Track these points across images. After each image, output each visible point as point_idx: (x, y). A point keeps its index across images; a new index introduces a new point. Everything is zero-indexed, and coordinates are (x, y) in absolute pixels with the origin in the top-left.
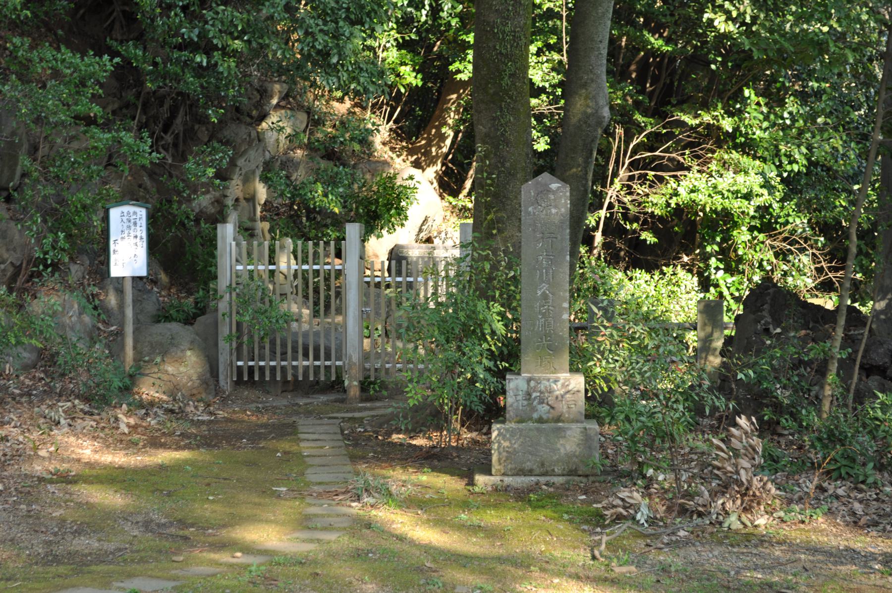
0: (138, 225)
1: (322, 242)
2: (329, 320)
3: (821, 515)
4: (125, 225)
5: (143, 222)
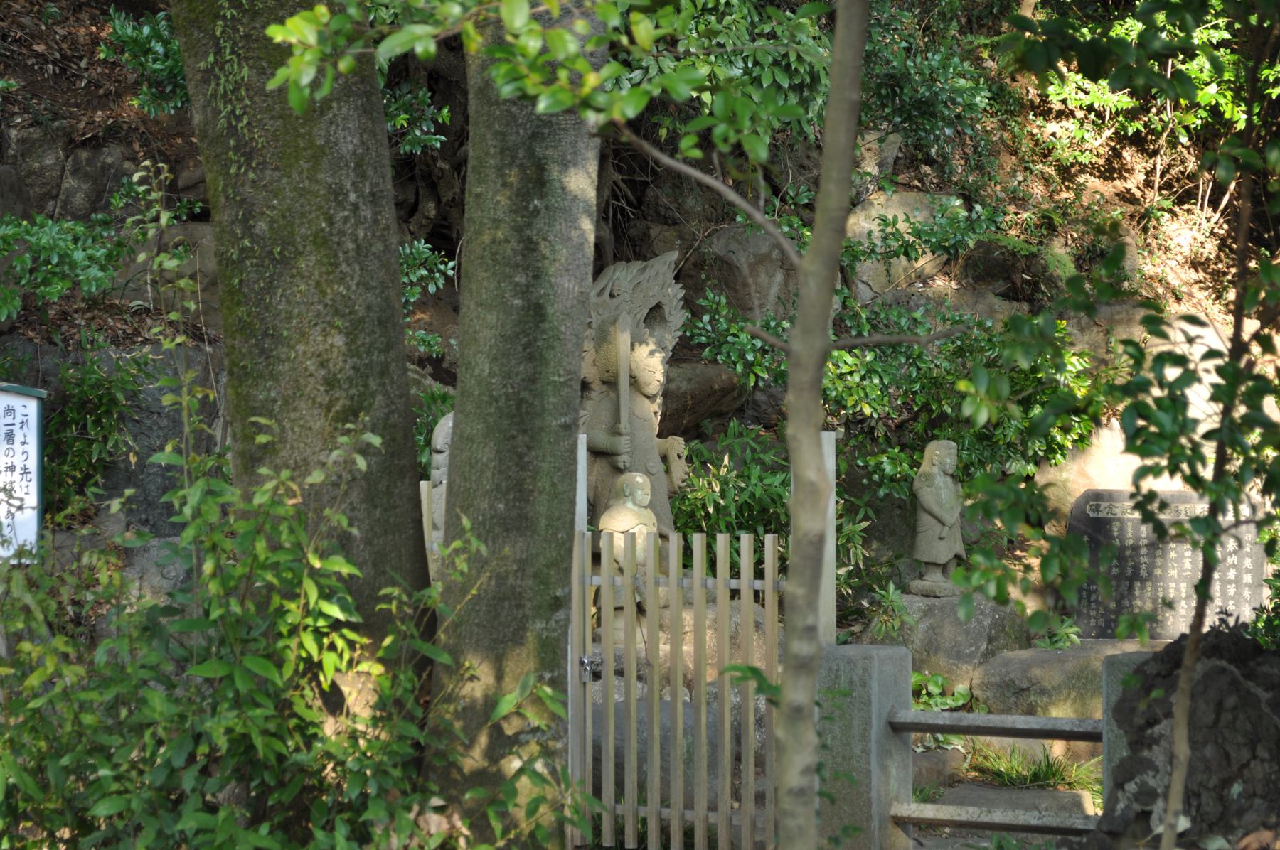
0: (19, 438)
2: (543, 522)
3: (282, 73)
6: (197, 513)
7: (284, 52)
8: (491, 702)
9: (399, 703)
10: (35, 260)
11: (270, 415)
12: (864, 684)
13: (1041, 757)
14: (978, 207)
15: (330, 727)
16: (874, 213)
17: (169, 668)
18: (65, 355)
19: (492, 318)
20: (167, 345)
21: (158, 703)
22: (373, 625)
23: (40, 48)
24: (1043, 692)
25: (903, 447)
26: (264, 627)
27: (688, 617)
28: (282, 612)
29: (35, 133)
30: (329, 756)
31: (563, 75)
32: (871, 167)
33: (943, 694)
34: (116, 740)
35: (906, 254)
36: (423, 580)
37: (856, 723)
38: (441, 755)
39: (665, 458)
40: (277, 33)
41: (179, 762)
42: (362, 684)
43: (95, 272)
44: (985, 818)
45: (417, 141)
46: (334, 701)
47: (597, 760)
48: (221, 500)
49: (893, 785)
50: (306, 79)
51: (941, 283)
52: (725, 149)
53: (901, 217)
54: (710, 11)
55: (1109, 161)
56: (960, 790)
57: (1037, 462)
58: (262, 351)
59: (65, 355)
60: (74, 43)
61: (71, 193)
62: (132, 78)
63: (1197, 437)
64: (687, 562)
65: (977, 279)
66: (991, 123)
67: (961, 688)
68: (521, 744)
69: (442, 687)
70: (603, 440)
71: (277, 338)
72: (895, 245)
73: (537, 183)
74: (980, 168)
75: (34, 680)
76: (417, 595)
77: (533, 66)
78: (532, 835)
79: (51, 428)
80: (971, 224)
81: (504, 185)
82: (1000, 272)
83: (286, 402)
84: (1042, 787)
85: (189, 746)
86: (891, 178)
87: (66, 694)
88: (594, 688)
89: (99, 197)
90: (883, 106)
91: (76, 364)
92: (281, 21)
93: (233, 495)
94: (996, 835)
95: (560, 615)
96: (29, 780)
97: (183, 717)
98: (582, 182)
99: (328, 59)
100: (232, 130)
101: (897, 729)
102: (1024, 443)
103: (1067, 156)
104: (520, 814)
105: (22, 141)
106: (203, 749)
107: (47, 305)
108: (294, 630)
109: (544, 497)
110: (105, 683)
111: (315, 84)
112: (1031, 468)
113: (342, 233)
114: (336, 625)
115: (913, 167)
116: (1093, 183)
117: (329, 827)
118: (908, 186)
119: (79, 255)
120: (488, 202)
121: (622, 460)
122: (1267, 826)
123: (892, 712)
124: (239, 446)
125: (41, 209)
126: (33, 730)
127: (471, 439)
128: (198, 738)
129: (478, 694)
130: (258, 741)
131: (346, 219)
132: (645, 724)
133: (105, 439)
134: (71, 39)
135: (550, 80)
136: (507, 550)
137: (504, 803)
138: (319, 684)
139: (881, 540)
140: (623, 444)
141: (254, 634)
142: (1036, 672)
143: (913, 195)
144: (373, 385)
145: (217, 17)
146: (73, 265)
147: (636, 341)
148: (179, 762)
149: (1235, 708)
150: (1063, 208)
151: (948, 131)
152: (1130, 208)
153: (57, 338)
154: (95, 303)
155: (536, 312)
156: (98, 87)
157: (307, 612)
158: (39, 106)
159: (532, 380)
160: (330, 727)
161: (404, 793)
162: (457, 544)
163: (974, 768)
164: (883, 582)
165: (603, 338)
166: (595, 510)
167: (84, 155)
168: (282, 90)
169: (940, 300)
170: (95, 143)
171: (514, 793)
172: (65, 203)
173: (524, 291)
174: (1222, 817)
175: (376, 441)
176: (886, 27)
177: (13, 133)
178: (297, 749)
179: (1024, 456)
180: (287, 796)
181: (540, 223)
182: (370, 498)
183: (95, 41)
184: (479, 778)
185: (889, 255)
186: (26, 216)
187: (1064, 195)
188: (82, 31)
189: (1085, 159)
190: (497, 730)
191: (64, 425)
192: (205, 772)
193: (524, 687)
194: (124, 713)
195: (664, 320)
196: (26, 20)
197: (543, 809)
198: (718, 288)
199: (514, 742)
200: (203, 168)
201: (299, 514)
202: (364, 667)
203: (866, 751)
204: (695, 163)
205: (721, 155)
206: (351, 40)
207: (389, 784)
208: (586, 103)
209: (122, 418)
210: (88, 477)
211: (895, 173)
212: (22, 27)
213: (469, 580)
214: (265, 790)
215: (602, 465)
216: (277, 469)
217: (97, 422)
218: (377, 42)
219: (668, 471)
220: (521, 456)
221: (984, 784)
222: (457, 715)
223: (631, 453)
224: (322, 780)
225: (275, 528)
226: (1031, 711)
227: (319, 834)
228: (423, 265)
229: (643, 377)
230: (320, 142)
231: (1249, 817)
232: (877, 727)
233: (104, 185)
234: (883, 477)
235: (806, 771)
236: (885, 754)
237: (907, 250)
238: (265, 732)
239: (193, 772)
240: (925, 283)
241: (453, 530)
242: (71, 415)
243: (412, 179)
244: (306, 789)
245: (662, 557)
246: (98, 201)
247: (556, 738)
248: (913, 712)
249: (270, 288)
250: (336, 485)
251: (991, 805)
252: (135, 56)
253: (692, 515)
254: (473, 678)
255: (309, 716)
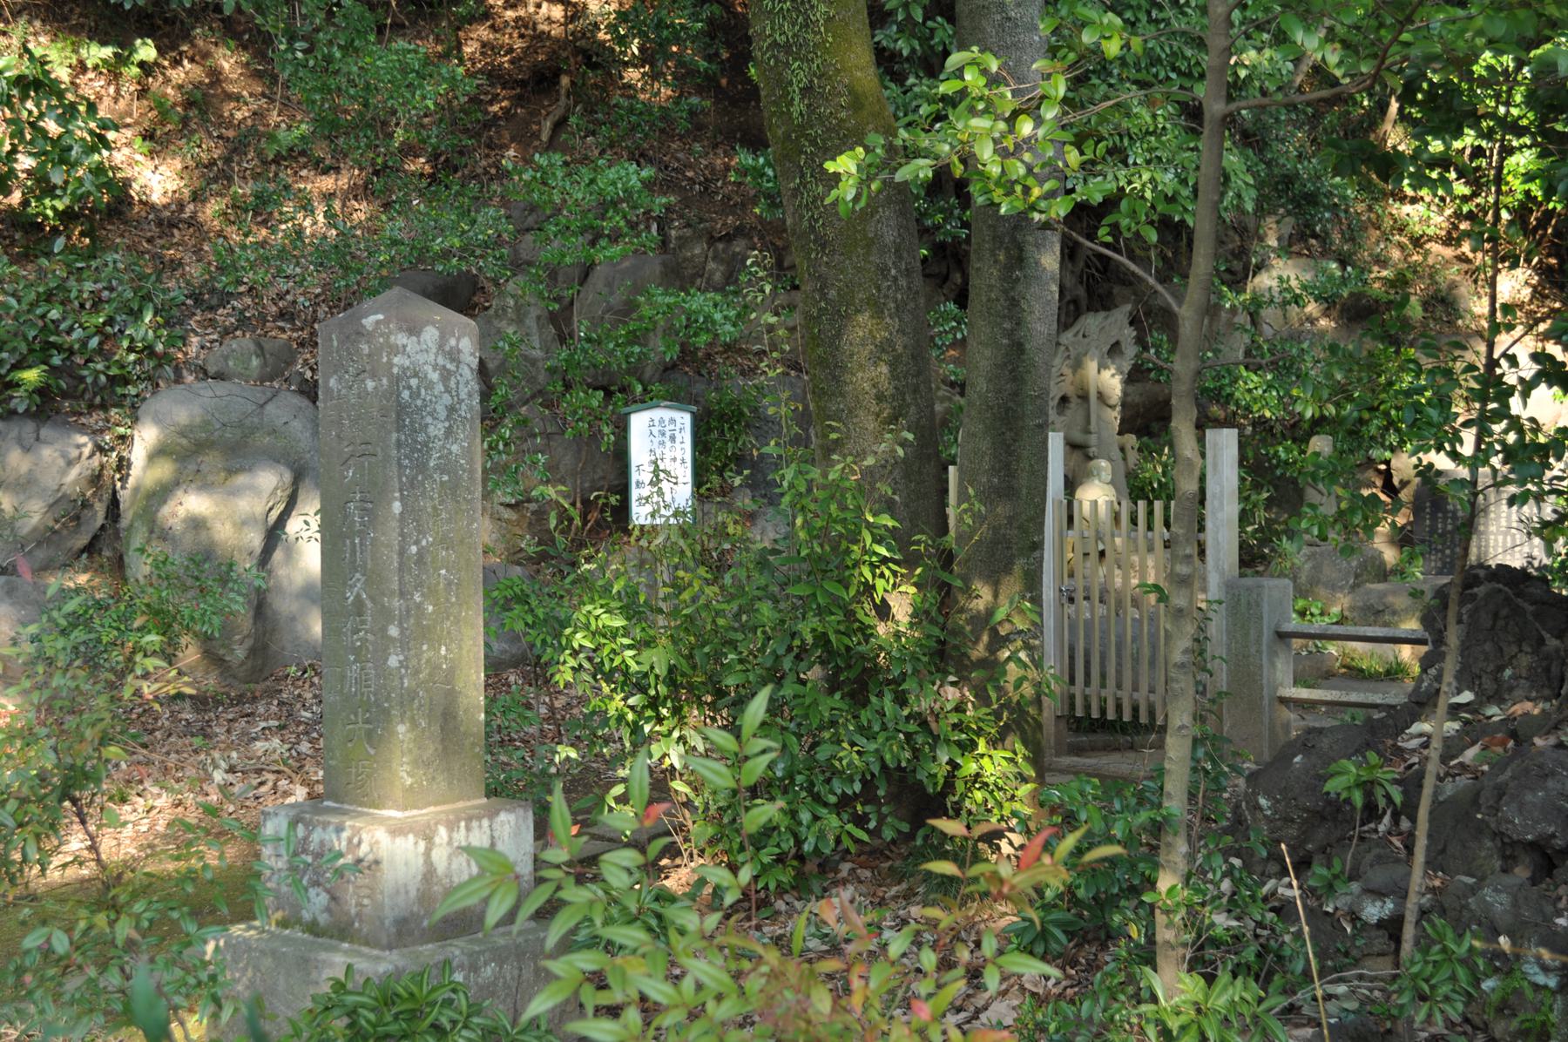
0: (678, 440)
1: (135, 115)
2: (1024, 491)
3: (834, 193)
4: (656, 441)
5: (687, 437)
6: (791, 486)
7: (837, 177)
8: (990, 612)
9: (927, 612)
10: (688, 319)
11: (839, 420)
12: (1258, 605)
13: (1392, 658)
14: (1349, 269)
15: (882, 629)
16: (1275, 273)
17: (775, 589)
18: (710, 382)
19: (988, 353)
20: (771, 374)
21: (766, 610)
22: (910, 561)
23: (690, 174)
24: (1394, 613)
25: (1294, 440)
26: (837, 562)
27: (1135, 559)
28: (848, 552)
29: (688, 232)
30: (881, 648)
31: (1018, 188)
32: (1273, 242)
33: (1322, 614)
34: (740, 636)
35: (1297, 303)
36: (944, 530)
37: (1252, 632)
38: (956, 647)
39: (1122, 449)
40: (831, 167)
41: (781, 651)
42: (902, 601)
43: (729, 328)
44: (1344, 699)
45: (947, 233)
46: (884, 611)
47: (1072, 658)
48: (809, 477)
49: (1279, 675)
50: (849, 197)
51: (1323, 322)
52: (1127, 235)
53: (1293, 277)
54: (1151, 134)
55: (1449, 233)
56: (1333, 681)
57: (1392, 449)
58: (834, 377)
59: (710, 382)
60: (713, 171)
61: (712, 273)
62: (752, 193)
63: (1457, 426)
64: (1134, 521)
65: (1349, 320)
66: (1360, 207)
67: (1335, 610)
68: (1011, 642)
69: (957, 602)
70: (1078, 437)
71: (844, 368)
72: (1288, 296)
73: (1018, 259)
74: (1352, 240)
75: (686, 596)
76: (939, 540)
77: (998, 183)
78: (1018, 703)
79: (701, 432)
80: (1344, 281)
81: (996, 262)
82: (1357, 311)
83: (850, 412)
84: (1393, 680)
85: (788, 640)
86: (1287, 249)
87: (707, 606)
88: (1070, 609)
89: (731, 275)
90: (1280, 197)
91: (716, 389)
92: (833, 159)
93: (815, 473)
94: (1351, 710)
95: (1037, 554)
96: (683, 661)
97: (783, 622)
98: (1050, 260)
99: (864, 182)
100: (812, 228)
101: (1283, 636)
102: (1383, 436)
103: (1419, 230)
104: (1010, 687)
105: (679, 238)
106: (797, 642)
107: (697, 349)
108: (856, 564)
109: (1025, 474)
110: (732, 597)
111: (856, 199)
112: (1388, 454)
113: (886, 296)
114: (885, 560)
115: (1300, 242)
116: (1435, 247)
117: (880, 695)
118: (1299, 254)
119: (718, 316)
120: (985, 274)
121: (1092, 451)
122: (1529, 699)
123: (1278, 625)
124: (820, 441)
125: (692, 284)
126: (687, 630)
127: (974, 435)
128: (793, 635)
129: (981, 607)
130: (833, 638)
131: (889, 288)
132: (1105, 634)
133: (737, 440)
134: (711, 167)
135: (1009, 193)
136: (999, 510)
137: (998, 680)
138: (873, 600)
139: (1279, 506)
140: (1093, 439)
141: (831, 566)
142: (1390, 599)
143: (1303, 260)
144: (908, 399)
145: (801, 152)
146: (714, 322)
147: (1102, 366)
148: (781, 651)
149: (1506, 617)
150: (1414, 268)
151: (1327, 215)
152: (1465, 266)
153: (704, 372)
154: (728, 347)
155: (1018, 348)
156: (729, 199)
157: (865, 551)
158: (691, 214)
159: (1016, 394)
160: (882, 629)
161: (931, 673)
162: (965, 506)
163: (1344, 666)
164: (1278, 535)
165: (1078, 365)
166: (1071, 485)
167: (720, 246)
168: (835, 203)
169: (1322, 333)
170: (728, 239)
171: (1005, 673)
172: (709, 279)
173: (1010, 334)
174: (1497, 692)
175: (910, 437)
176: (1283, 141)
177: (673, 233)
178: (859, 643)
179: (1383, 445)
180: (852, 674)
181: (1020, 287)
182: (907, 476)
183: (727, 168)
184: (981, 663)
185: (1285, 303)
186: (683, 289)
187: (1415, 258)
188: (719, 161)
189: (1430, 231)
190: (994, 632)
191: (710, 430)
192: (798, 658)
193: (1011, 603)
194: (744, 618)
195: (1122, 353)
196: (680, 155)
197: (1025, 685)
198: (1161, 330)
199: (1006, 640)
200: (795, 257)
201: (859, 486)
202: (903, 588)
203: (1259, 651)
204: (1107, 245)
205: (1126, 239)
206: (880, 169)
207: (920, 667)
208: (1033, 208)
209: (748, 426)
210: (725, 465)
211: (1290, 245)
212: (678, 160)
213: (973, 531)
214: (838, 670)
215: (1077, 455)
216: (845, 456)
217: (731, 428)
218: (896, 170)
219: (1125, 459)
220: (1009, 446)
221: (1351, 677)
222: (968, 622)
223: (1098, 446)
224: (876, 665)
225: (843, 496)
226: (1386, 625)
227: (874, 699)
228: (954, 319)
229: (1107, 391)
230: (871, 235)
231: (1518, 693)
232: (1267, 635)
233: (734, 267)
234: (1279, 461)
235: (1186, 651)
236: (1273, 654)
237: (1297, 299)
238: (838, 632)
239: (791, 657)
240: (1312, 323)
241: (963, 496)
242: (714, 424)
243: (945, 257)
244: (865, 670)
245: (1116, 518)
246: (730, 277)
247: (1036, 637)
248: (1294, 623)
249: (839, 335)
250: (884, 467)
251: (1349, 689)
252: (754, 179)
253: (1142, 489)
254: (978, 597)
255: (867, 621)
